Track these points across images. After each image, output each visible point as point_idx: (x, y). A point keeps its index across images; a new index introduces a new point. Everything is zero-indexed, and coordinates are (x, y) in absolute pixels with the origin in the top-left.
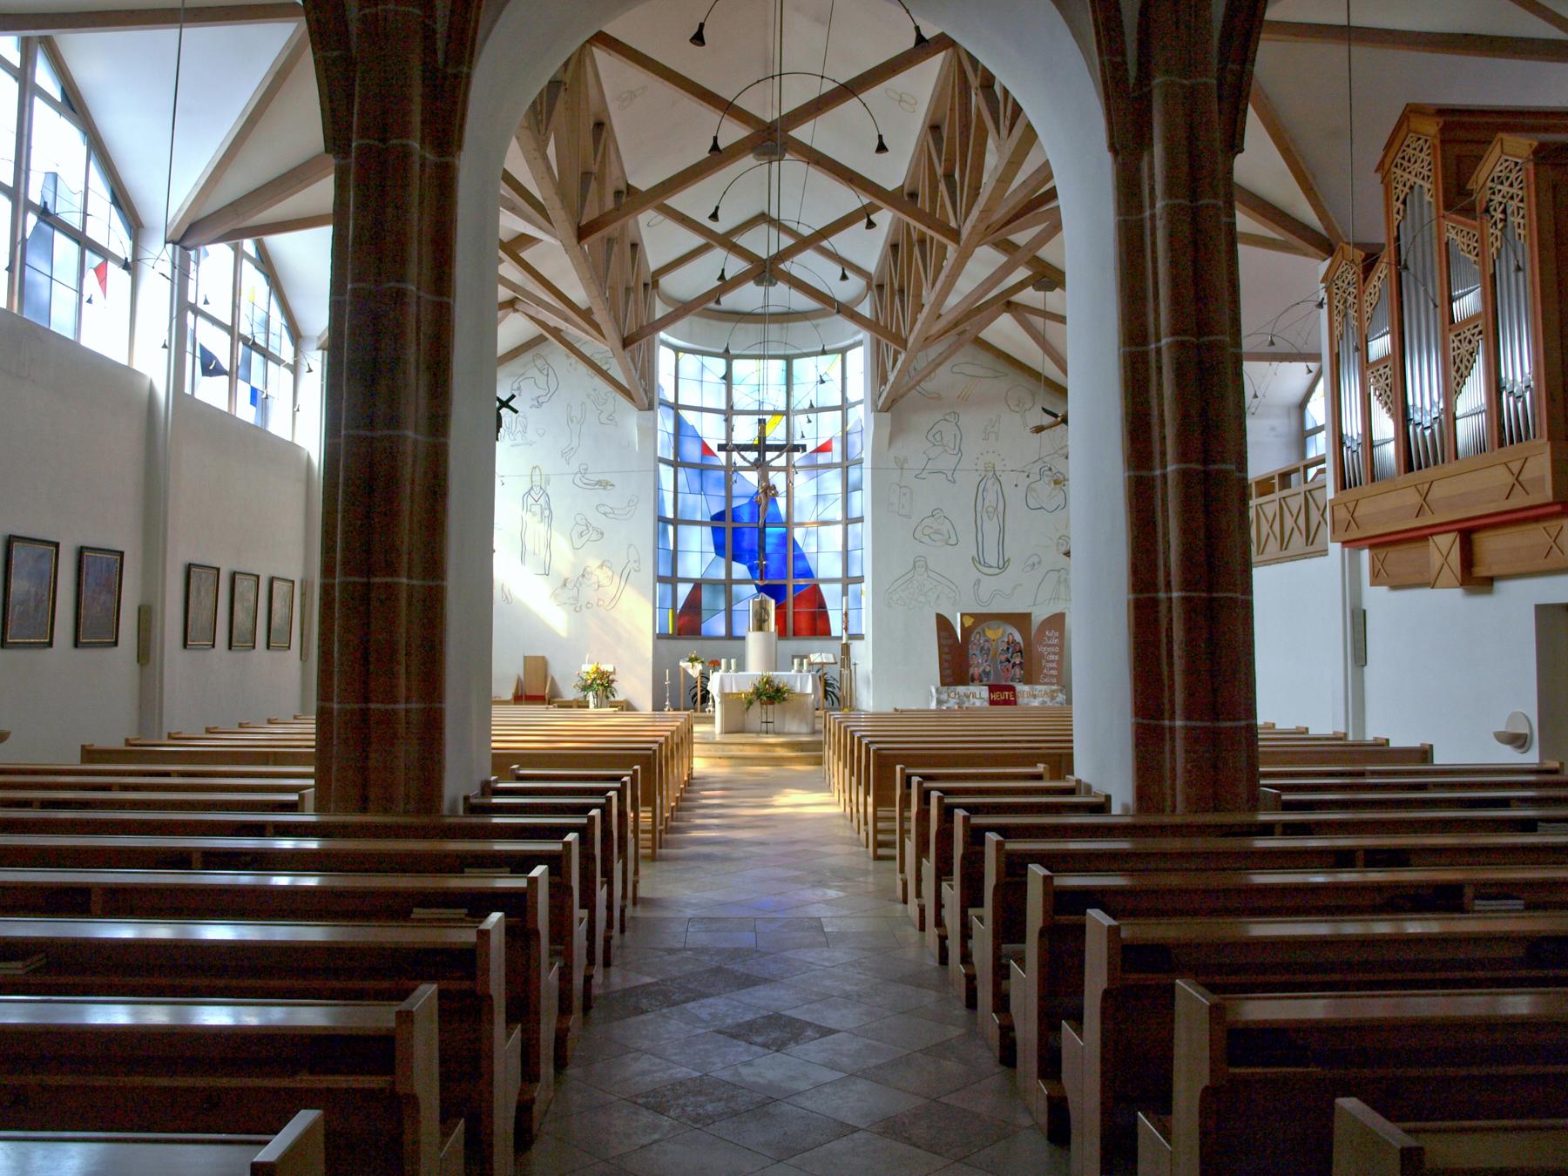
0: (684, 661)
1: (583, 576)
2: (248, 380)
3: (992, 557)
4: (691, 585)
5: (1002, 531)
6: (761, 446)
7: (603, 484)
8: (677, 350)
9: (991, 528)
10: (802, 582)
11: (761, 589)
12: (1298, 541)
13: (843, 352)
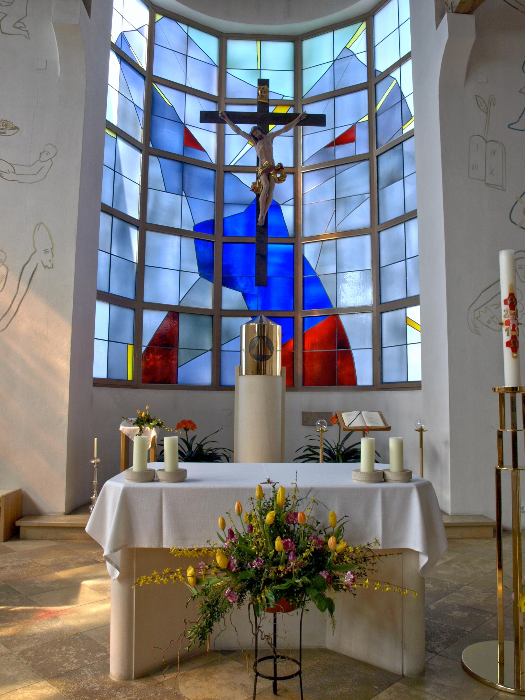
0: (128, 424)
10: (316, 313)
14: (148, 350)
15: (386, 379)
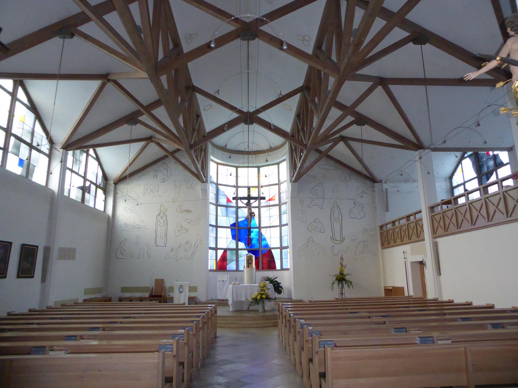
1: (180, 247)
2: (17, 155)
3: (338, 237)
4: (223, 251)
5: (341, 227)
6: (249, 198)
7: (188, 211)
8: (218, 164)
9: (337, 226)
11: (249, 251)
12: (414, 237)
13: (278, 164)
14: (219, 260)
15: (284, 268)
